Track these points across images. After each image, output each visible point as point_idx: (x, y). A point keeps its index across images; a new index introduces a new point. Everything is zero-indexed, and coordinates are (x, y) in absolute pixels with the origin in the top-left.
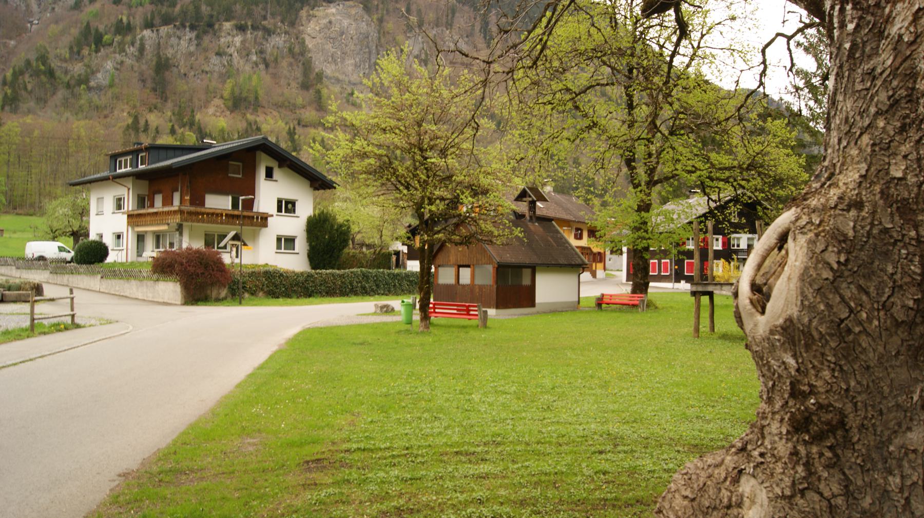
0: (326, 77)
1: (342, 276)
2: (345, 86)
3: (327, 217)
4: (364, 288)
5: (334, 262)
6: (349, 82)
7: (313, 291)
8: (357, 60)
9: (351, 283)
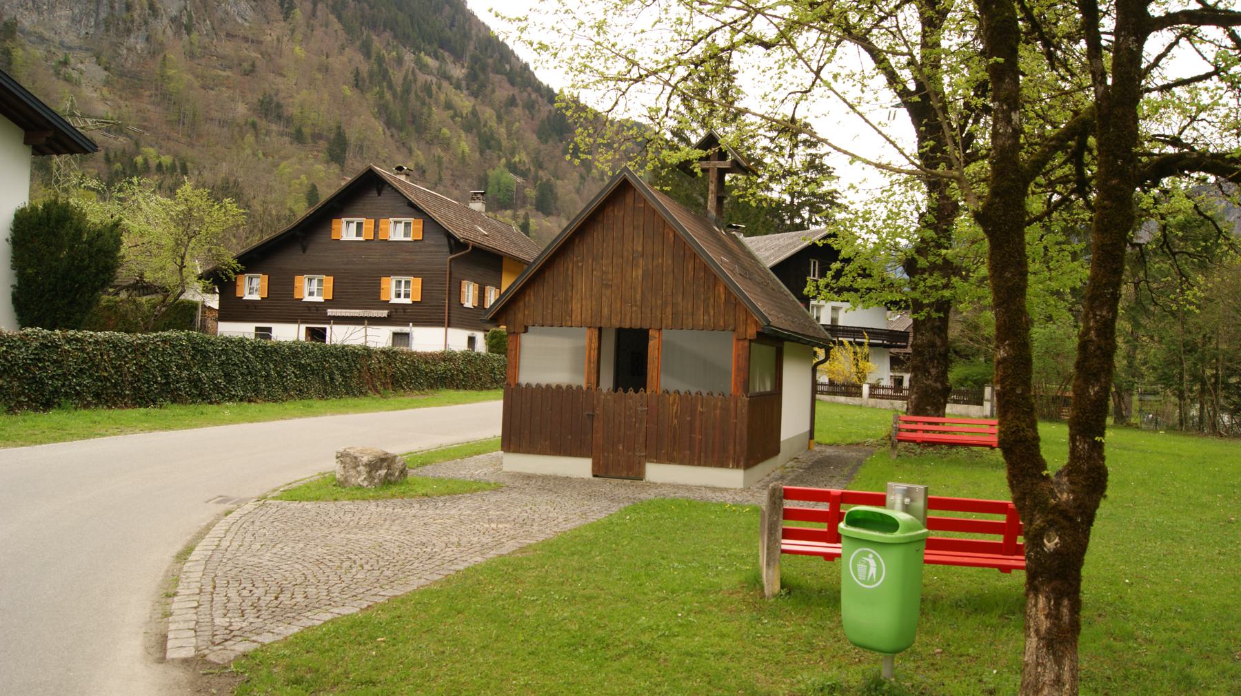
0: (22, 32)
1: (137, 349)
2: (53, 49)
3: (66, 211)
4: (195, 382)
5: (78, 316)
6: (62, 44)
7: (56, 391)
8: (77, 11)
9: (164, 369)
